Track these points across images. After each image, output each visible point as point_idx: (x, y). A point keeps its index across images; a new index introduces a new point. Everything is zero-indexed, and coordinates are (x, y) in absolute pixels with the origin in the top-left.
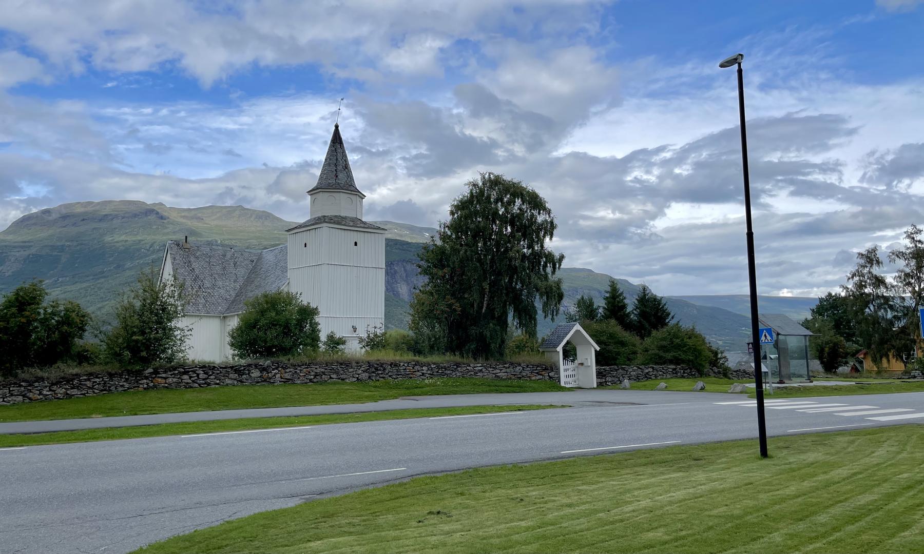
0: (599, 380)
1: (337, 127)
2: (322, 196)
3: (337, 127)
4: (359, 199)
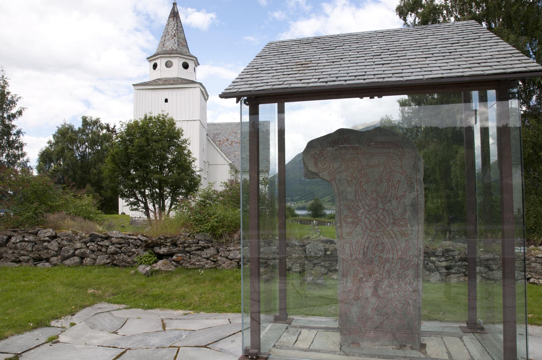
3: (175, 4)
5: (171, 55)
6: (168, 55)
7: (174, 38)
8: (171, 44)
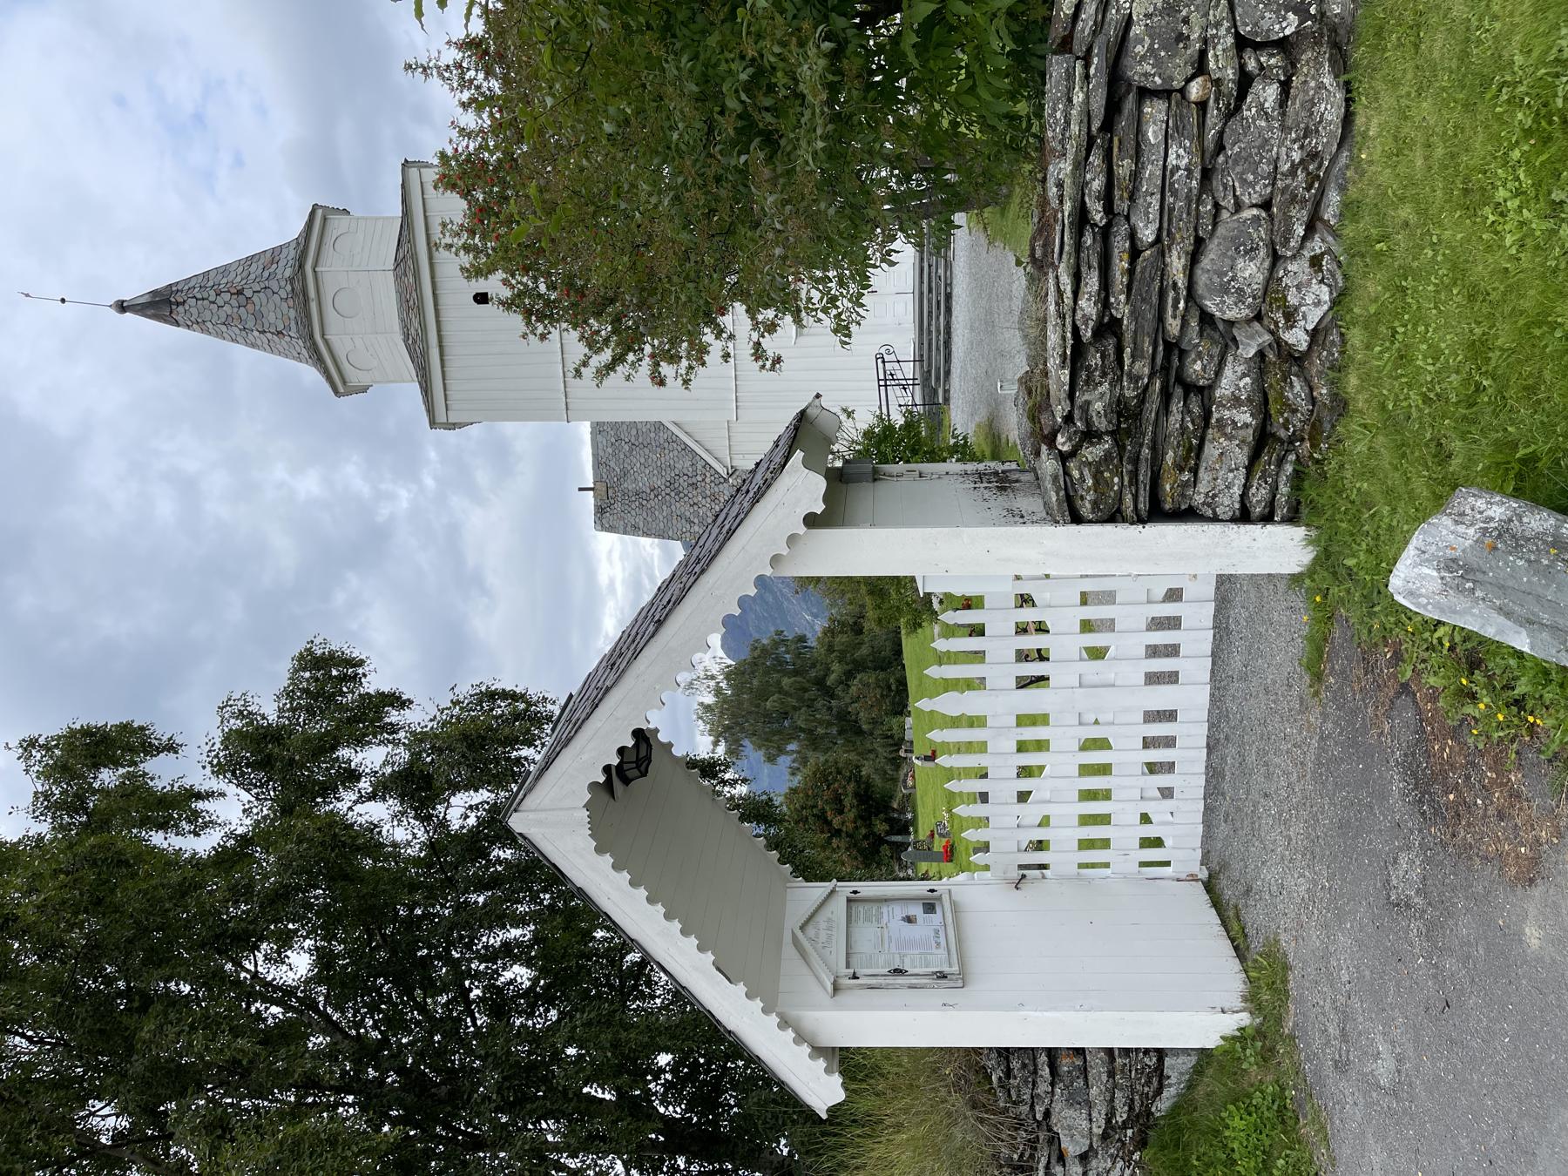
0: (1224, 468)
1: (122, 307)
2: (343, 335)
3: (122, 307)
4: (337, 225)
5: (312, 293)
6: (314, 306)
7: (248, 293)
8: (277, 310)
